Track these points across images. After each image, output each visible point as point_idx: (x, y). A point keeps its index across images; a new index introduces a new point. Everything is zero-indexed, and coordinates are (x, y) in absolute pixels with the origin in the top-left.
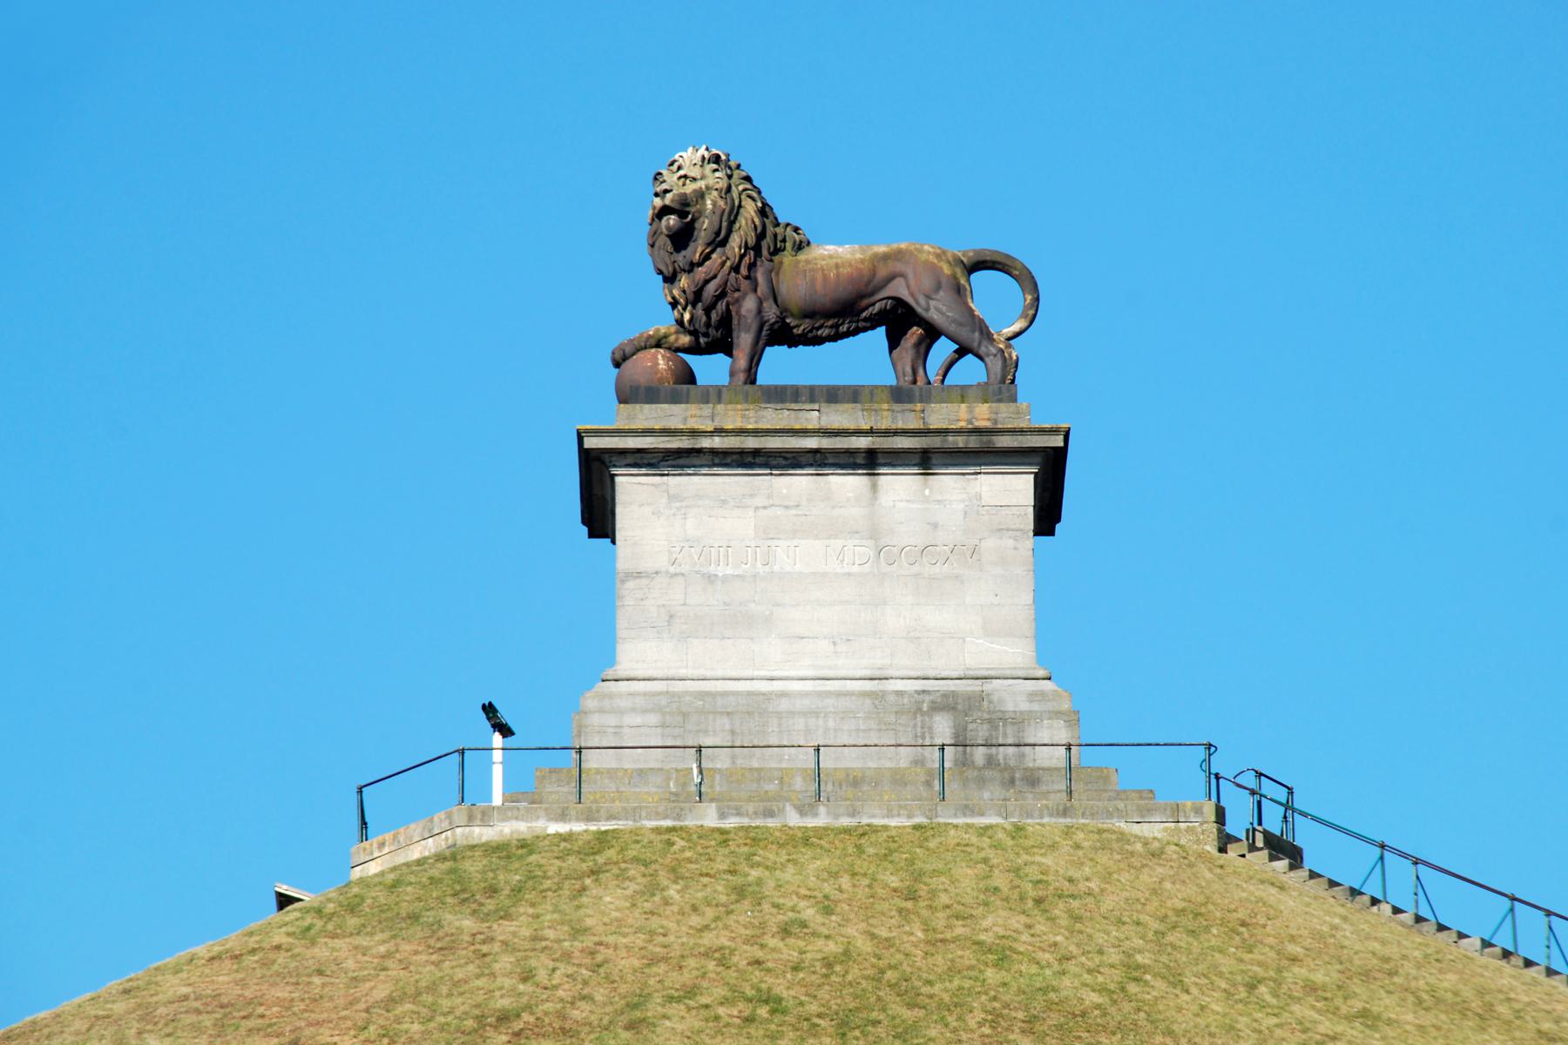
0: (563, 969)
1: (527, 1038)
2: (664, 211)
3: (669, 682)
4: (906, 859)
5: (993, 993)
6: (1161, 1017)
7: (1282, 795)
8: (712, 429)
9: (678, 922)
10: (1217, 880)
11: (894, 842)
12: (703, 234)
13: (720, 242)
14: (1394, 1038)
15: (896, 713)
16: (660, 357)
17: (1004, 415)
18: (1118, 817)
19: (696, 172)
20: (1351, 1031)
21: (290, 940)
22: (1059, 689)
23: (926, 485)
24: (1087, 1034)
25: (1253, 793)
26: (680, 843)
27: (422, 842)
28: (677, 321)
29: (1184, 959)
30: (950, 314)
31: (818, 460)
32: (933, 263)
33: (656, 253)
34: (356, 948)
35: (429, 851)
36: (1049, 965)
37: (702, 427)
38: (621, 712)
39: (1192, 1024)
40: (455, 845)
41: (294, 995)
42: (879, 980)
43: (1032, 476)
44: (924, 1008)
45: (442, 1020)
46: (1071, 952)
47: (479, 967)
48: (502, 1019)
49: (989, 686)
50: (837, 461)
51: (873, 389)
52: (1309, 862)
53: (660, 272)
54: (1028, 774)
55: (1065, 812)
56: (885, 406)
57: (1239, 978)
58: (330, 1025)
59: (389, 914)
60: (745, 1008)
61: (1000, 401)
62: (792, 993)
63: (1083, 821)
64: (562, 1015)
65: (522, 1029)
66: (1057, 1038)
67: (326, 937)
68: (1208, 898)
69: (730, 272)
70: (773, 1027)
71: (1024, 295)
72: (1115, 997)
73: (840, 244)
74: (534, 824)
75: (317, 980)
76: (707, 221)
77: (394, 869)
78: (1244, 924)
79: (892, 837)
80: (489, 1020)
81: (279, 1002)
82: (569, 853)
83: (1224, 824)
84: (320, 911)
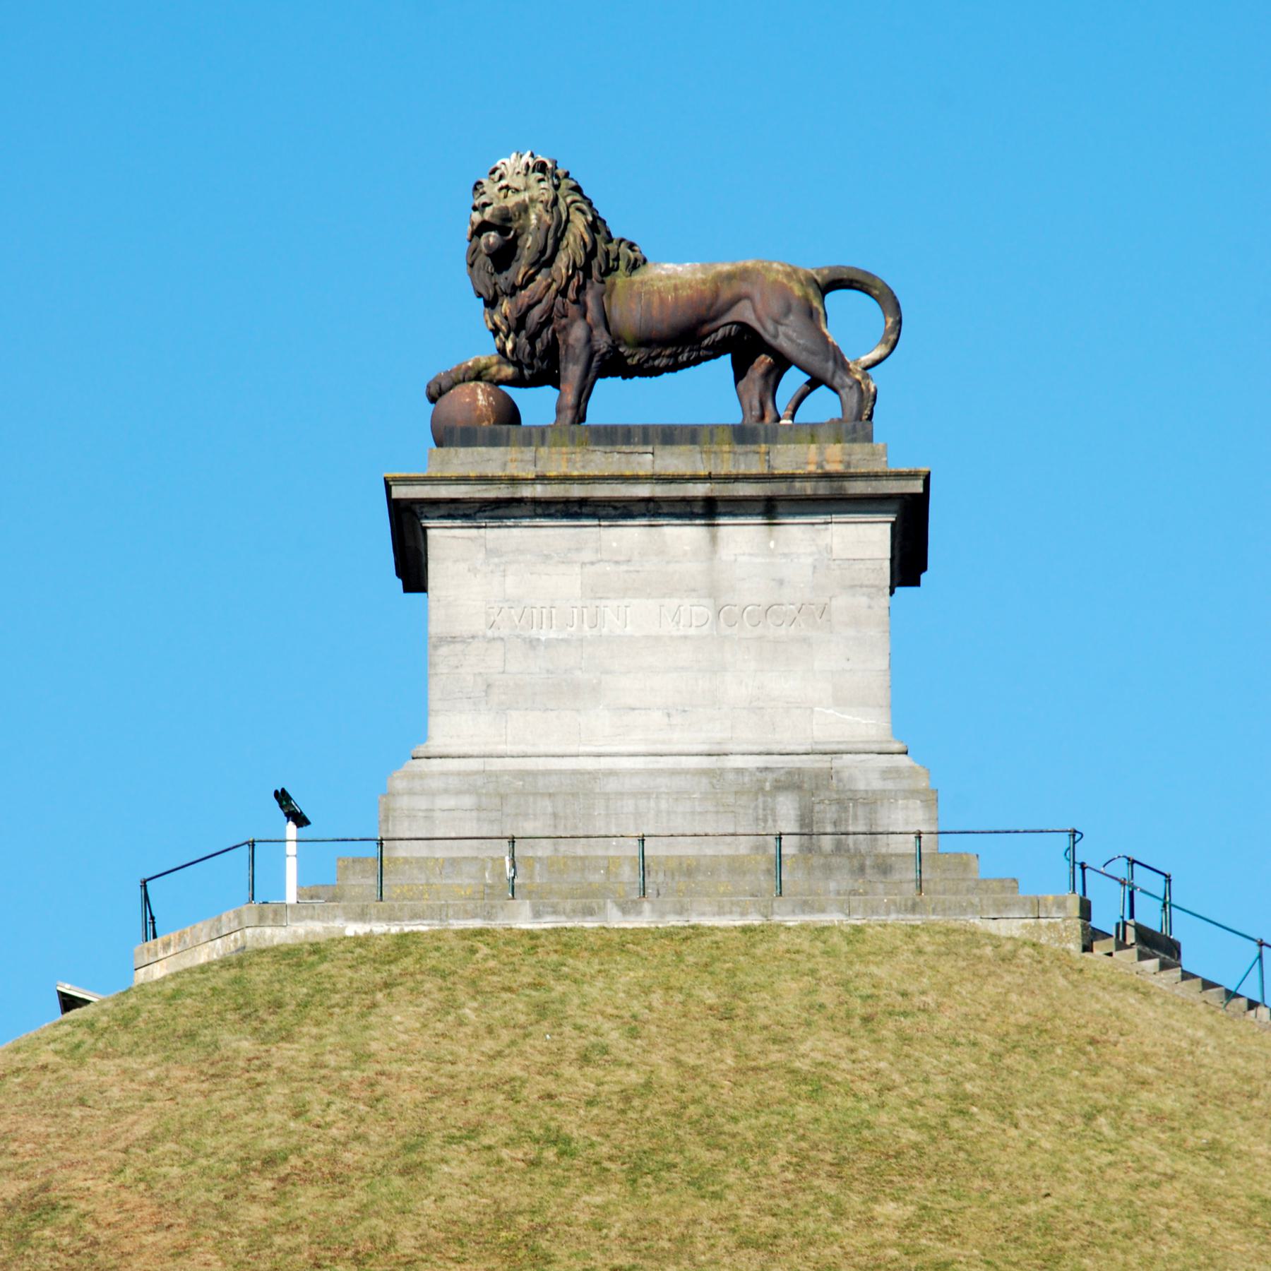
0: (340, 1104)
1: (293, 1184)
2: (481, 229)
3: (486, 759)
4: (728, 970)
5: (801, 1131)
6: (983, 1157)
7: (1157, 885)
8: (533, 476)
9: (470, 1047)
10: (1070, 987)
11: (718, 948)
12: (526, 252)
13: (544, 262)
14: (1241, 1174)
15: (736, 793)
16: (479, 391)
17: (859, 456)
18: (973, 913)
19: (518, 182)
20: (1192, 1168)
21: (58, 1059)
22: (916, 765)
23: (770, 536)
24: (900, 1178)
25: (1123, 883)
26: (484, 950)
27: (210, 943)
28: (499, 350)
29: (1020, 1086)
30: (801, 342)
31: (651, 509)
32: (783, 284)
33: (476, 273)
34: (125, 1071)
35: (217, 955)
36: (867, 1098)
37: (522, 474)
38: (433, 794)
39: (1016, 1164)
40: (244, 948)
41: (51, 1130)
42: (679, 1117)
43: (888, 526)
44: (725, 1149)
45: (203, 1162)
46: (894, 1081)
47: (250, 1100)
48: (268, 1162)
49: (839, 762)
50: (672, 510)
51: (713, 430)
52: (1188, 962)
53: (480, 295)
54: (880, 861)
55: (914, 908)
56: (726, 448)
57: (1077, 1107)
58: (85, 1167)
59: (165, 1031)
60: (531, 1150)
61: (854, 440)
62: (583, 1132)
63: (934, 917)
64: (332, 1158)
65: (289, 1174)
66: (866, 1183)
67: (95, 1056)
68: (1056, 1011)
69: (556, 296)
70: (559, 1172)
71: (885, 317)
72: (935, 1133)
73: (679, 260)
74: (331, 924)
75: (77, 1112)
76: (530, 239)
77: (176, 975)
78: (1093, 1042)
79: (716, 942)
80: (254, 1163)
81: (34, 1138)
82: (363, 960)
83: (1089, 920)
84: (93, 1025)
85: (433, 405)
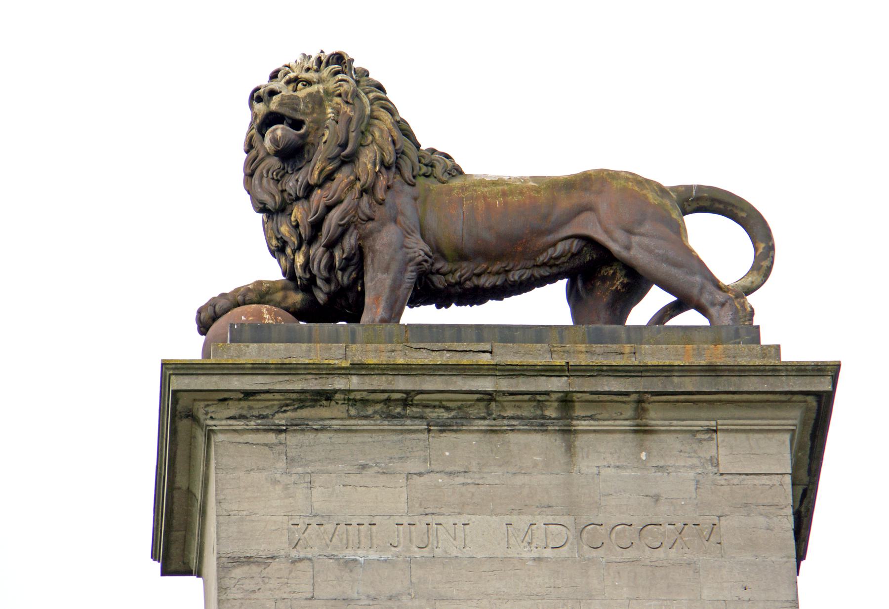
23: (641, 447)
43: (787, 437)
76: (327, 133)
85: (204, 337)
